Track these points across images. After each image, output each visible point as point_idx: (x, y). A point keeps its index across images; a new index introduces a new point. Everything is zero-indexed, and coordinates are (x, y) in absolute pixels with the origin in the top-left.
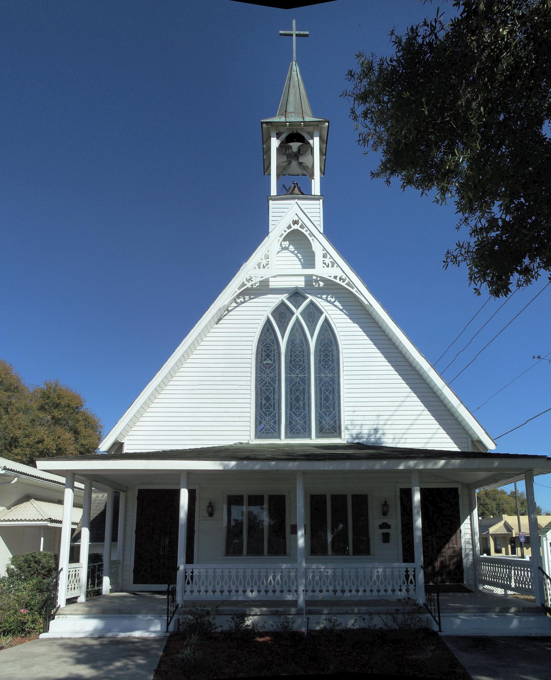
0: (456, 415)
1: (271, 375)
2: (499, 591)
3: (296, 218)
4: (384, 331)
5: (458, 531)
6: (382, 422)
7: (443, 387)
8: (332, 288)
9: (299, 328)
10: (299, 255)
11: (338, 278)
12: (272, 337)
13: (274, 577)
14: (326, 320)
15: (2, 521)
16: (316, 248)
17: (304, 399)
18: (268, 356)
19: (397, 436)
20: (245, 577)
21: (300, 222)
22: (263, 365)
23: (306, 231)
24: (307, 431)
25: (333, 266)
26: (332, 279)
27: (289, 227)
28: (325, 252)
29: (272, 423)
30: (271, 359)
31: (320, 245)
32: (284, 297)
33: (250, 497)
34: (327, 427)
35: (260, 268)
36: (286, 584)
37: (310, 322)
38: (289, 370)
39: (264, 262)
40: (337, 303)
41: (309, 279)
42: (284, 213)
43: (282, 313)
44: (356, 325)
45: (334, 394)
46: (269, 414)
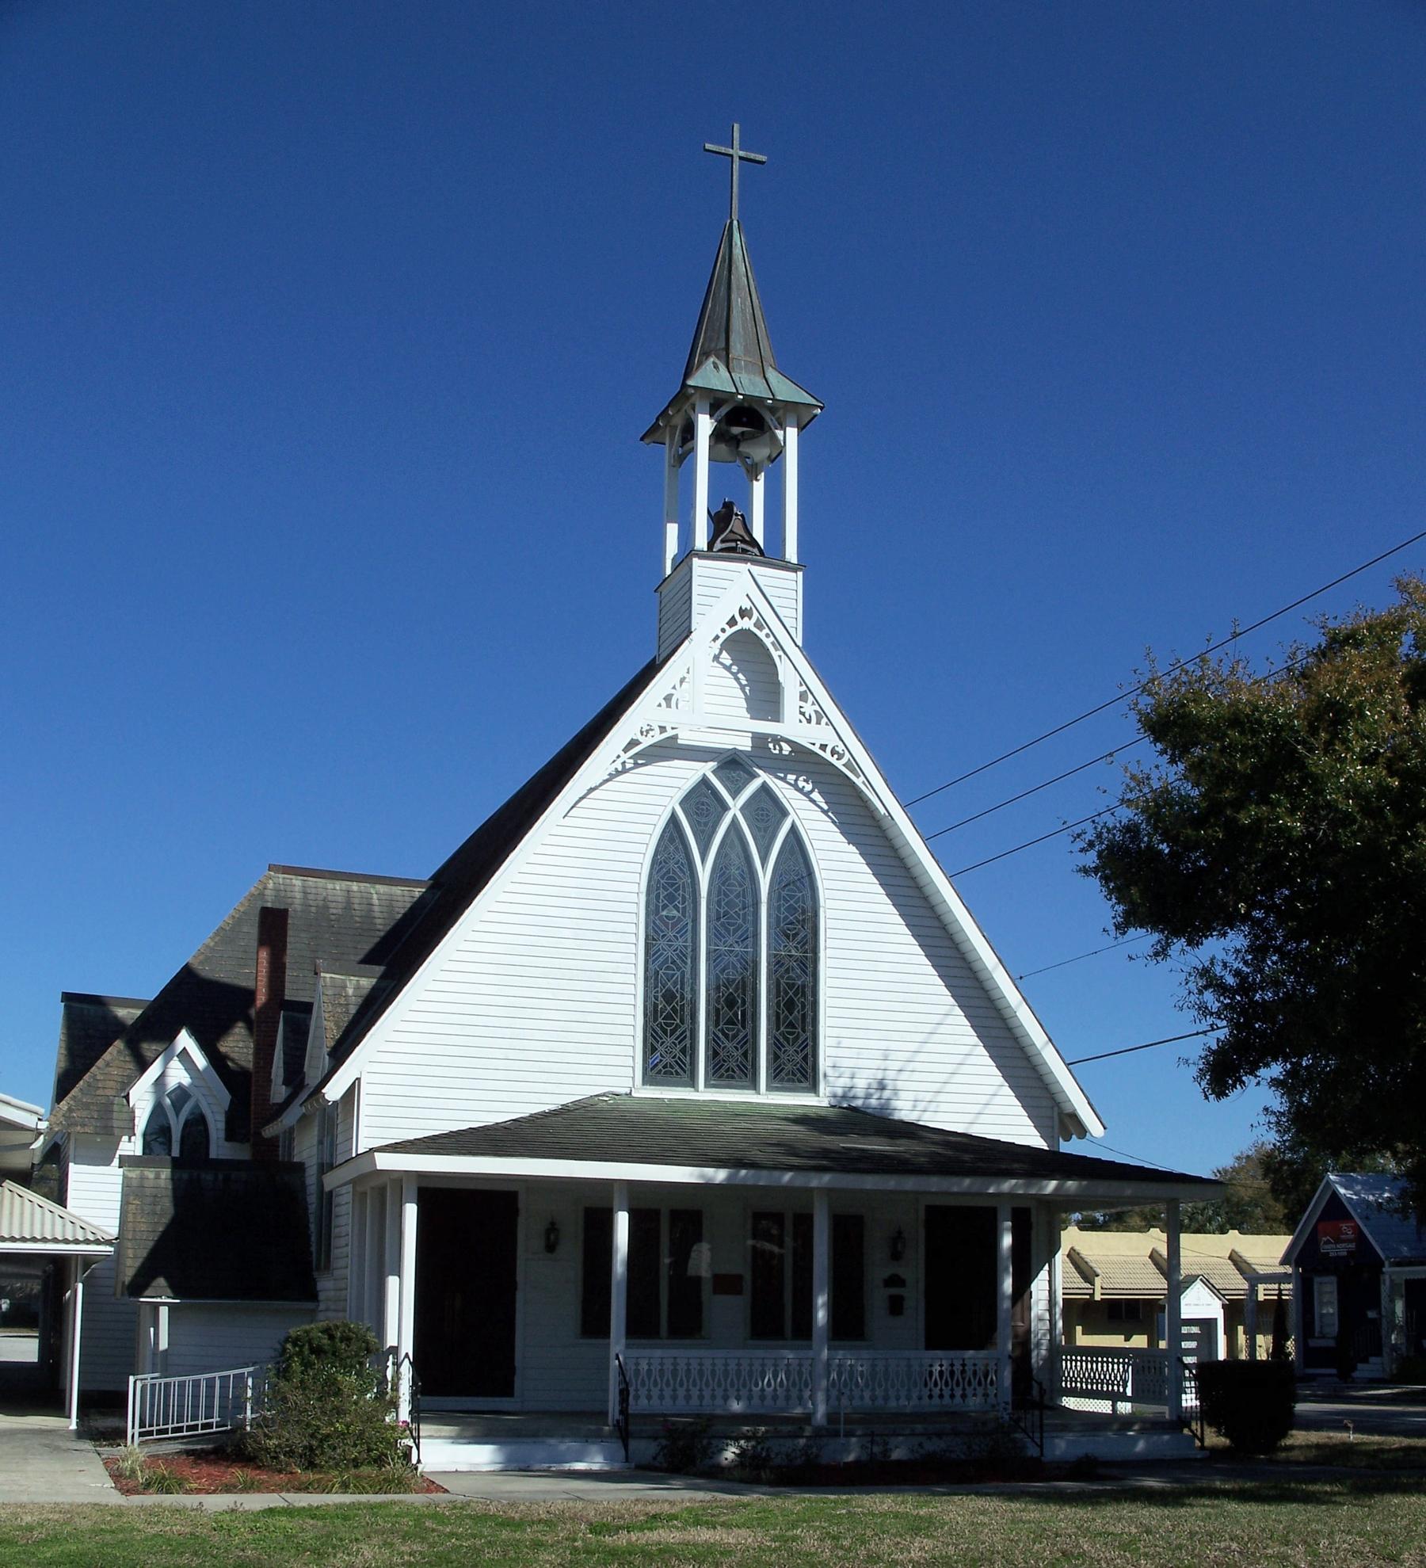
0: (1012, 1023)
1: (676, 944)
2: (1103, 1407)
3: (747, 605)
4: (932, 908)
5: (1026, 1296)
6: (897, 1065)
7: (1019, 1005)
8: (804, 762)
9: (737, 842)
10: (740, 676)
11: (829, 749)
12: (680, 857)
13: (775, 1376)
14: (794, 830)
15: (2, 1239)
16: (786, 676)
17: (744, 1002)
18: (671, 898)
19: (921, 1096)
20: (726, 1373)
21: (756, 615)
22: (661, 918)
23: (767, 636)
24: (750, 1075)
25: (818, 723)
26: (816, 749)
27: (732, 622)
28: (804, 688)
29: (677, 1051)
30: (676, 908)
31: (795, 672)
32: (707, 768)
34: (789, 1067)
35: (669, 706)
36: (794, 1384)
37: (759, 829)
38: (714, 935)
40: (816, 796)
41: (759, 740)
42: (721, 591)
43: (702, 804)
44: (852, 848)
45: (804, 994)
46: (673, 1032)
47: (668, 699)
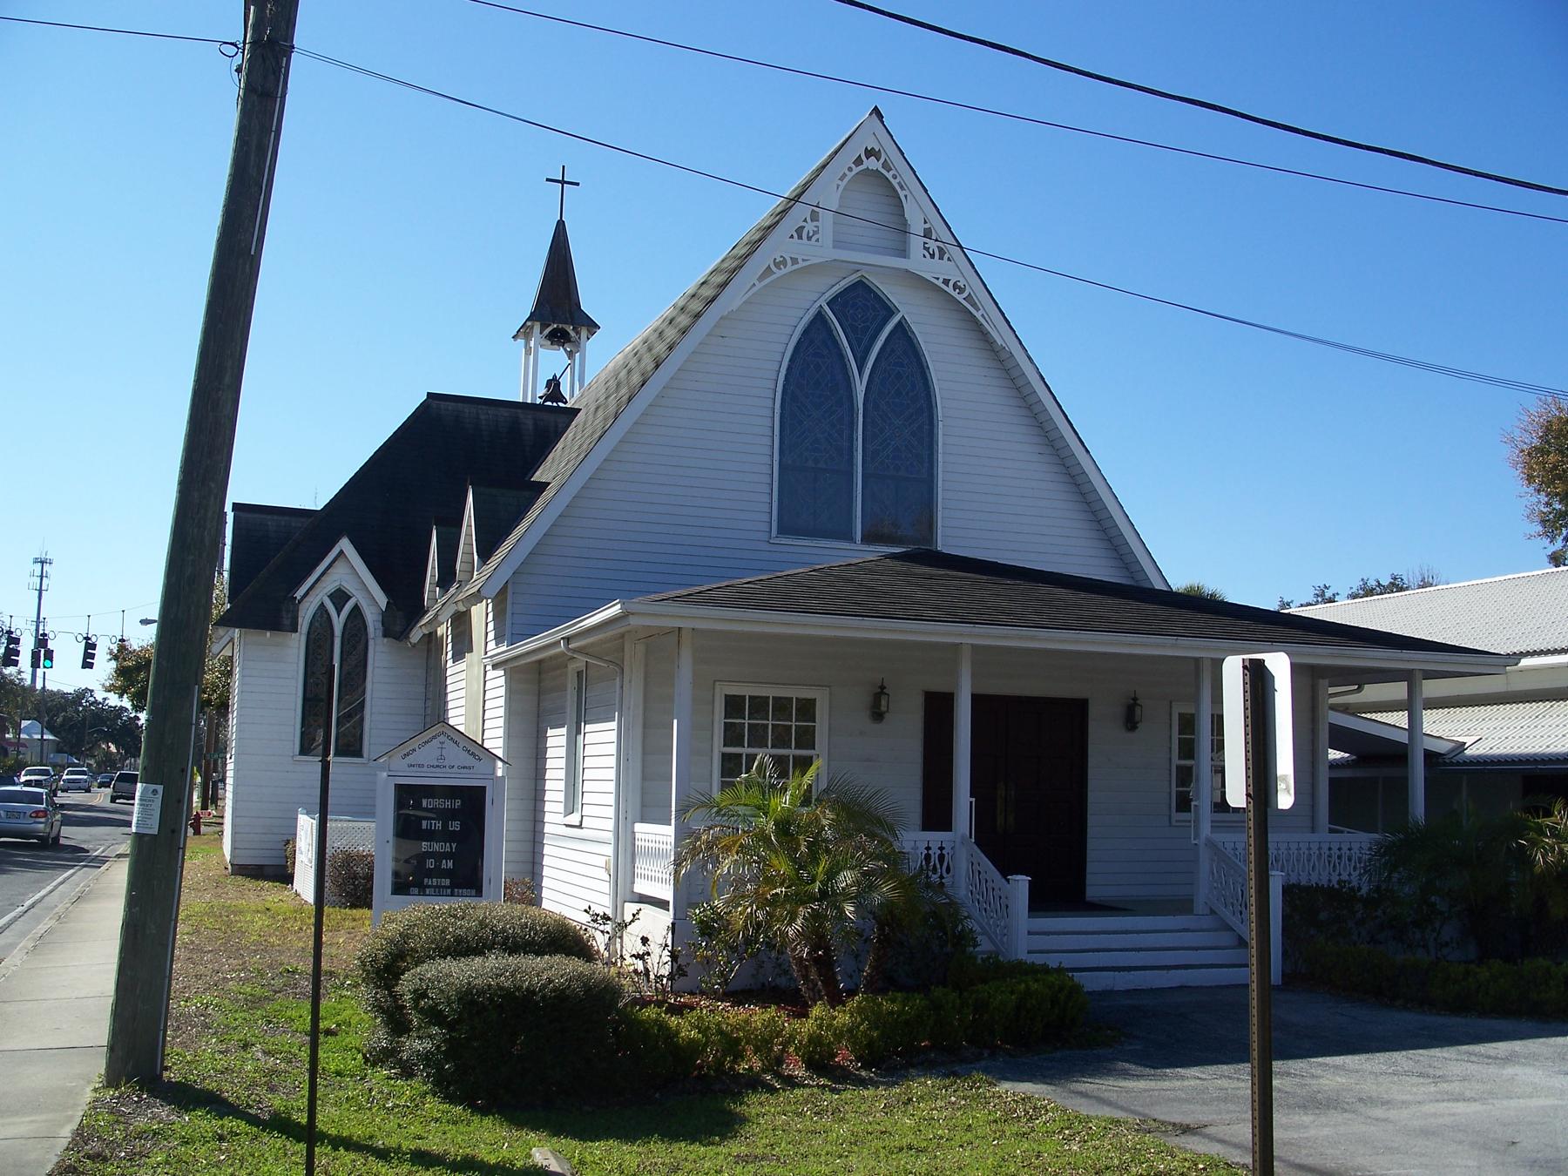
23: (895, 177)
25: (941, 258)
26: (939, 283)
33: (1189, 769)
35: (800, 237)
39: (810, 227)
47: (800, 230)
